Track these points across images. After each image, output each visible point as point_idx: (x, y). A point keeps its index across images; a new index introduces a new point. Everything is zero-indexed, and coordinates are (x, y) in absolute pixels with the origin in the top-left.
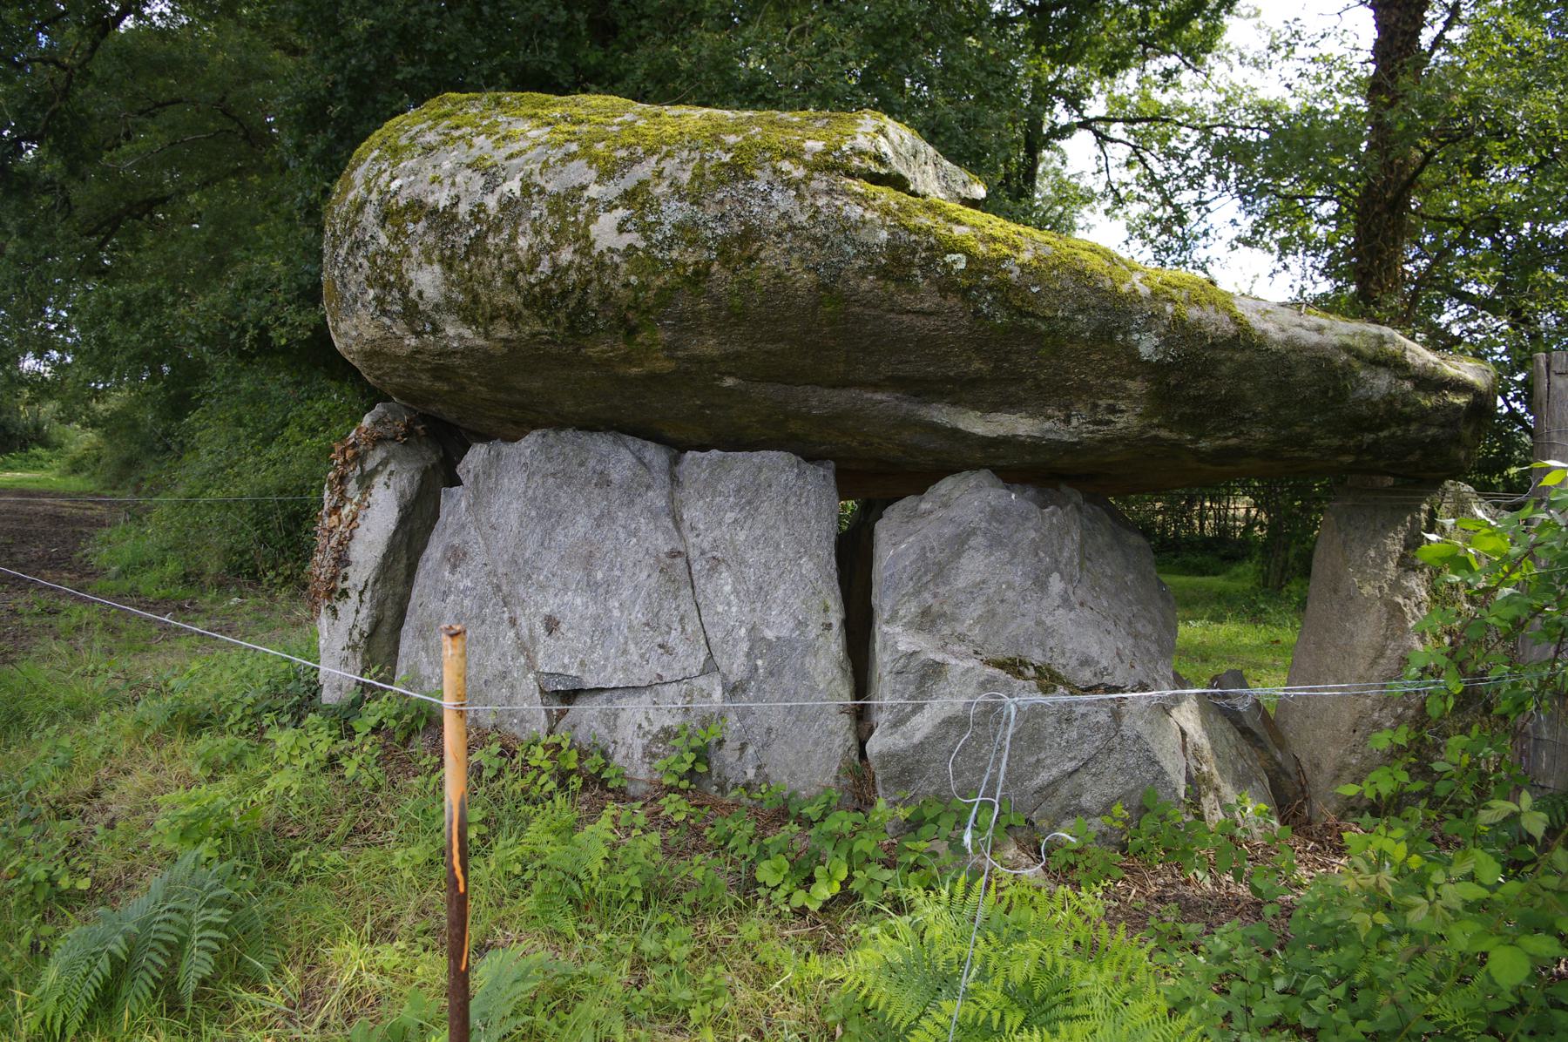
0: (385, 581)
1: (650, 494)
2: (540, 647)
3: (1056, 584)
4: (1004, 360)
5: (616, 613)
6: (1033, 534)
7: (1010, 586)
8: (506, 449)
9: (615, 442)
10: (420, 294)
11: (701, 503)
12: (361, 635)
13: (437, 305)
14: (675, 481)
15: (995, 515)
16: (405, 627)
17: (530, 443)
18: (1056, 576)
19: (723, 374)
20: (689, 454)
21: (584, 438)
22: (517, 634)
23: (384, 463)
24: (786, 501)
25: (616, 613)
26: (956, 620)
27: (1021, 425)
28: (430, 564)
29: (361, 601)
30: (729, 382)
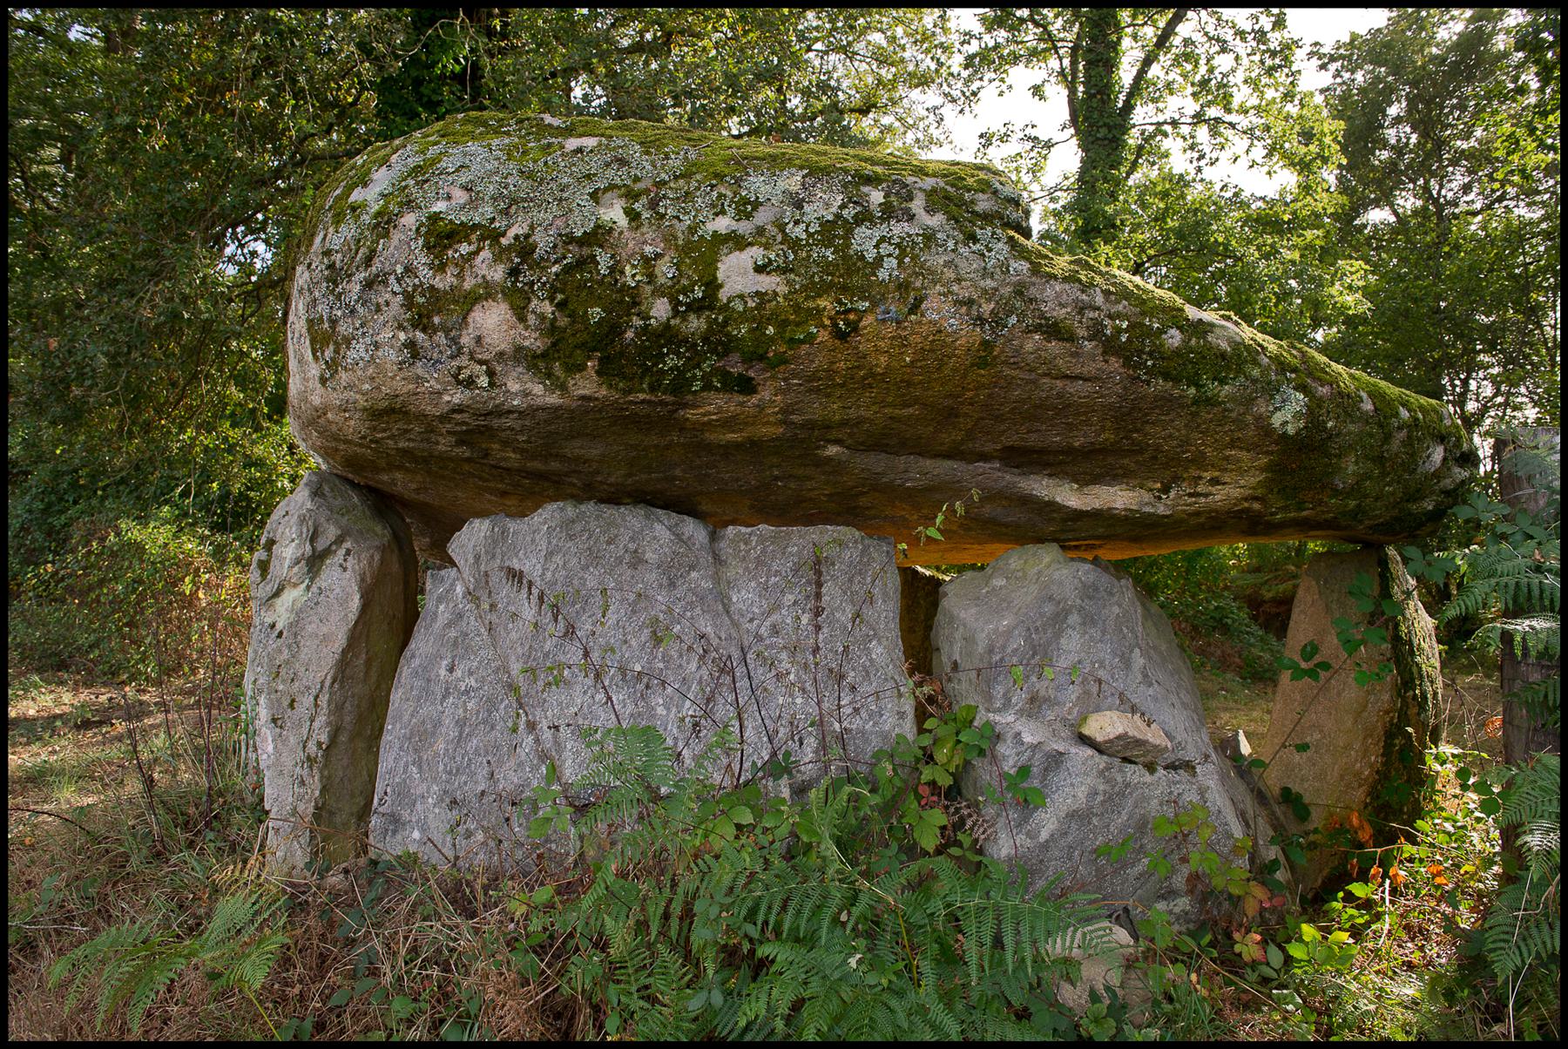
0: (342, 682)
1: (694, 574)
2: (567, 754)
3: (1138, 660)
4: (1137, 431)
5: (660, 711)
6: (1116, 610)
7: (1102, 665)
8: (513, 525)
9: (647, 517)
10: (479, 340)
11: (753, 584)
12: (319, 744)
13: (501, 354)
14: (718, 560)
15: (1089, 592)
16: (386, 737)
17: (547, 516)
18: (1137, 650)
19: (829, 441)
20: (731, 530)
21: (609, 511)
22: (537, 741)
23: (339, 541)
24: (851, 580)
25: (660, 711)
26: (1058, 704)
27: (1119, 498)
28: (416, 662)
29: (316, 705)
30: (832, 450)
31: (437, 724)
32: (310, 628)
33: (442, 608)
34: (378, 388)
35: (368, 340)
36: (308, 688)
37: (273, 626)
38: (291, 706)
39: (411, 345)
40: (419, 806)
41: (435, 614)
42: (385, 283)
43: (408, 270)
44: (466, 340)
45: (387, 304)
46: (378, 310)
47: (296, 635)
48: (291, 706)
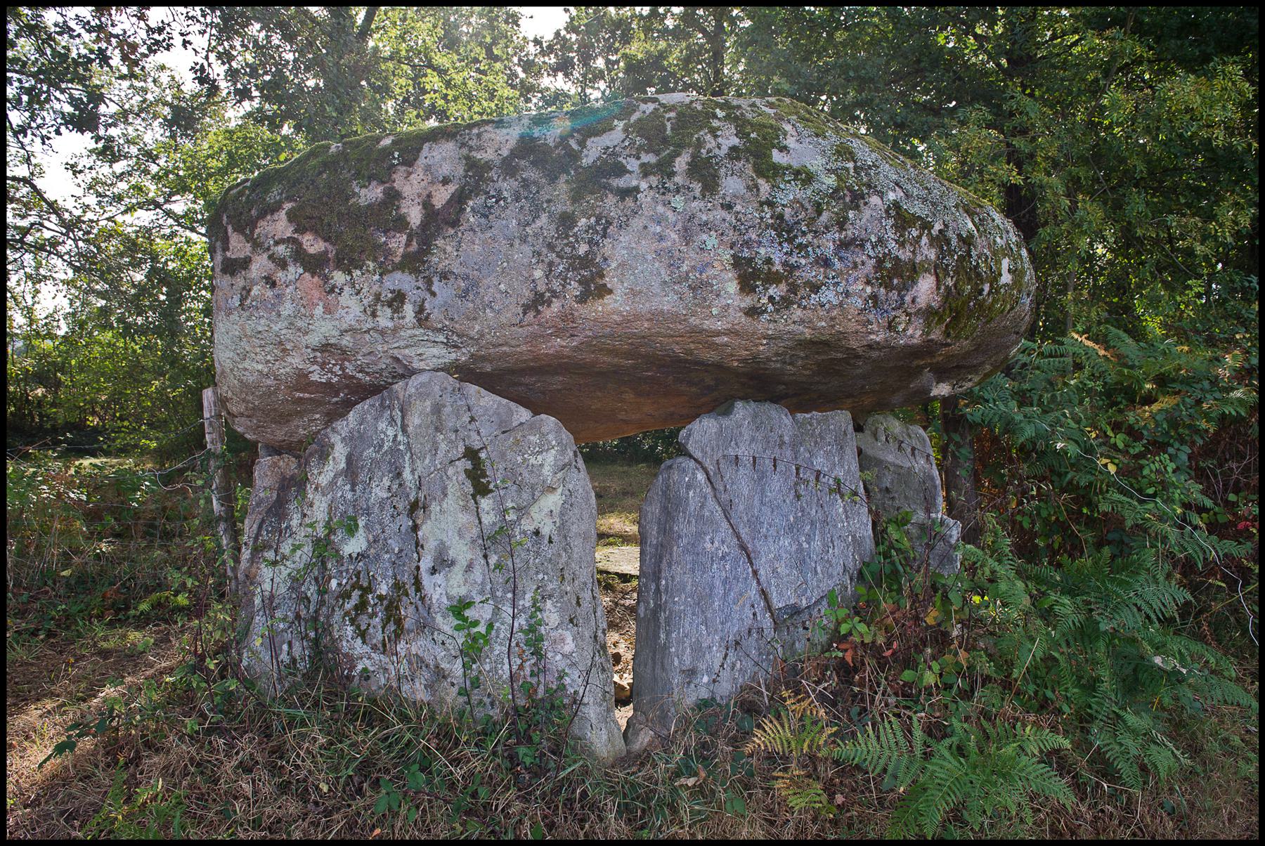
17: (742, 411)
31: (712, 587)
32: (574, 529)
33: (691, 493)
34: (833, 326)
35: (840, 289)
36: (585, 584)
37: (537, 533)
38: (578, 604)
39: (874, 297)
40: (708, 656)
41: (687, 499)
42: (862, 246)
43: (881, 241)
44: (908, 299)
45: (863, 263)
46: (855, 266)
47: (565, 537)
48: (578, 604)
